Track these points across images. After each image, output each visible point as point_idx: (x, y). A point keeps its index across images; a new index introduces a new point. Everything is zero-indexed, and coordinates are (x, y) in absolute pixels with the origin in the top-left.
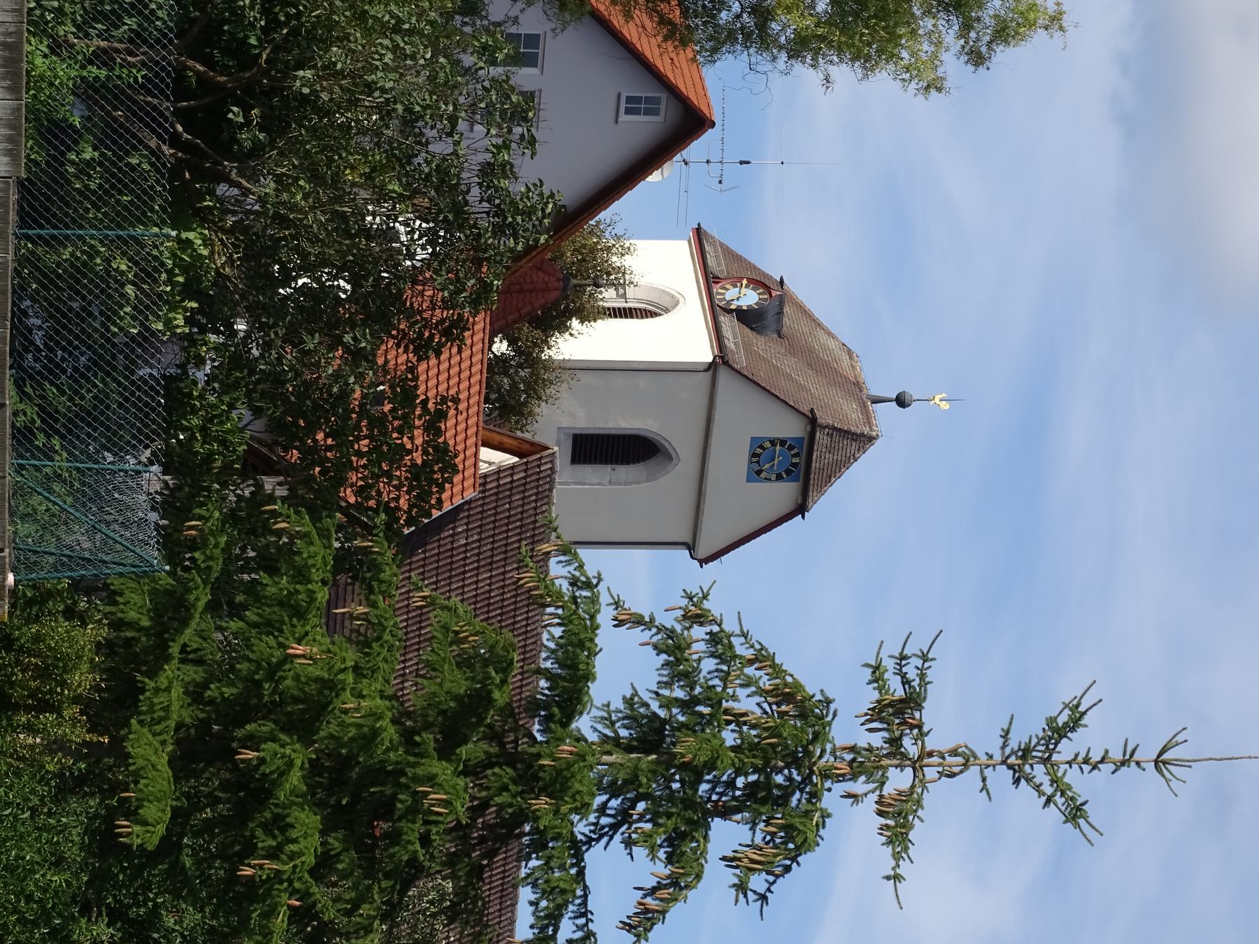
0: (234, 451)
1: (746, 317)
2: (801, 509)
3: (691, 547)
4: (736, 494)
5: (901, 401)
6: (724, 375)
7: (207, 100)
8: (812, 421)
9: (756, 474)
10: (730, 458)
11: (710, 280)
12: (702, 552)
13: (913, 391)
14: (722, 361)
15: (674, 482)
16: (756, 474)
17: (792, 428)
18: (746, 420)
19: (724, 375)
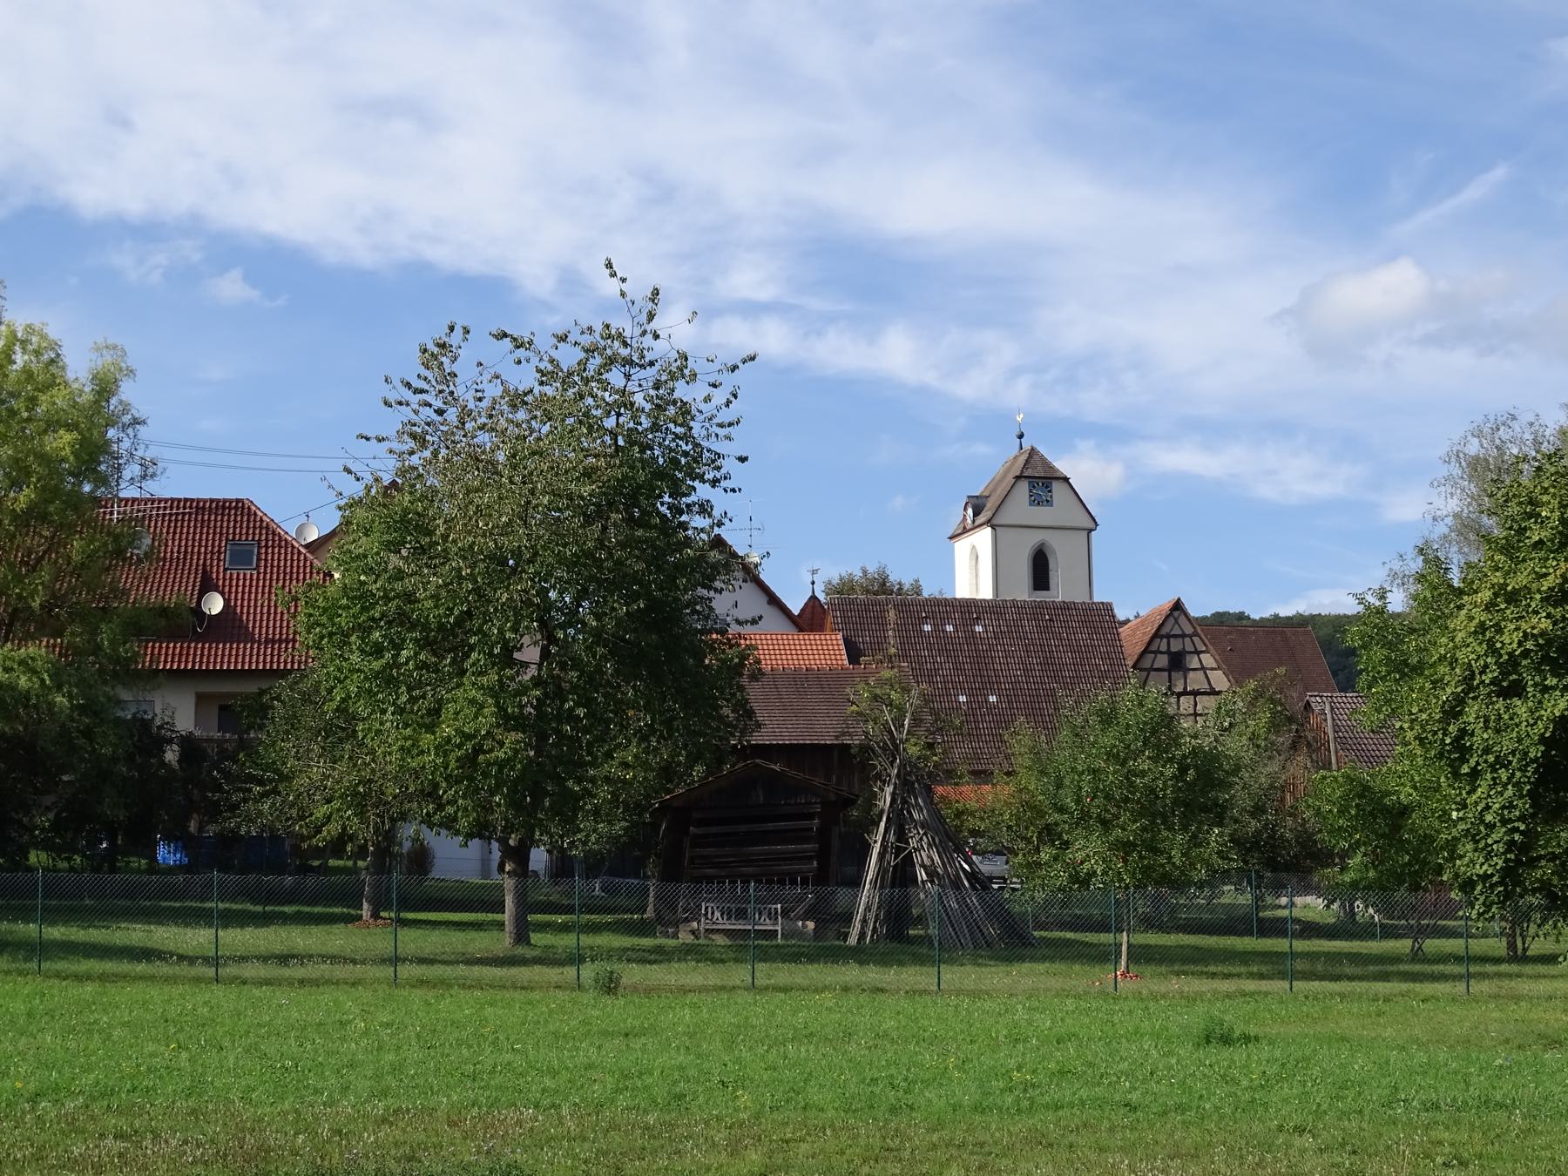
0: (295, 1152)
1: (976, 514)
2: (1066, 479)
3: (1090, 531)
4: (1060, 510)
5: (1021, 436)
6: (994, 522)
7: (651, 899)
8: (1018, 478)
9: (1049, 503)
10: (1042, 515)
11: (965, 531)
12: (1092, 525)
13: (1017, 432)
14: (988, 522)
15: (1055, 541)
16: (1049, 503)
17: (1024, 486)
18: (1020, 508)
19: (994, 522)
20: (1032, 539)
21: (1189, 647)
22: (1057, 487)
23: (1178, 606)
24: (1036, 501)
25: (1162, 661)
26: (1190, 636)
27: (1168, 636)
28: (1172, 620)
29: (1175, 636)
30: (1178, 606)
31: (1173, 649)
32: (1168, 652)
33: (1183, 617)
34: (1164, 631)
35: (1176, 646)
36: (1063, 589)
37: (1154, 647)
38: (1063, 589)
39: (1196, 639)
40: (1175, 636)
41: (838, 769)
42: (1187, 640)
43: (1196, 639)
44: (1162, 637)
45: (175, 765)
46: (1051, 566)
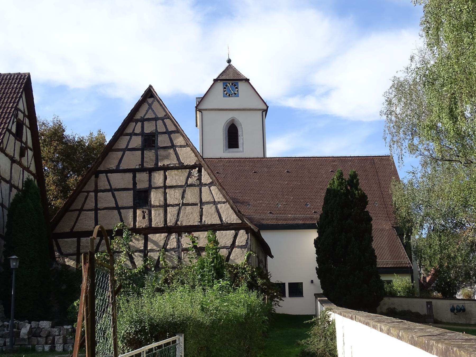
2: (247, 80)
8: (215, 81)
10: (232, 102)
13: (227, 59)
17: (220, 85)
20: (225, 118)
21: (161, 129)
22: (241, 85)
23: (150, 94)
24: (228, 94)
25: (137, 141)
26: (162, 119)
27: (143, 120)
28: (145, 106)
29: (149, 120)
30: (150, 94)
31: (147, 131)
32: (142, 134)
33: (156, 103)
34: (139, 115)
35: (149, 128)
36: (247, 149)
37: (129, 130)
38: (247, 149)
39: (167, 121)
40: (149, 120)
41: (201, 255)
42: (160, 122)
43: (167, 121)
44: (137, 121)
45: (427, 281)
46: (240, 133)
